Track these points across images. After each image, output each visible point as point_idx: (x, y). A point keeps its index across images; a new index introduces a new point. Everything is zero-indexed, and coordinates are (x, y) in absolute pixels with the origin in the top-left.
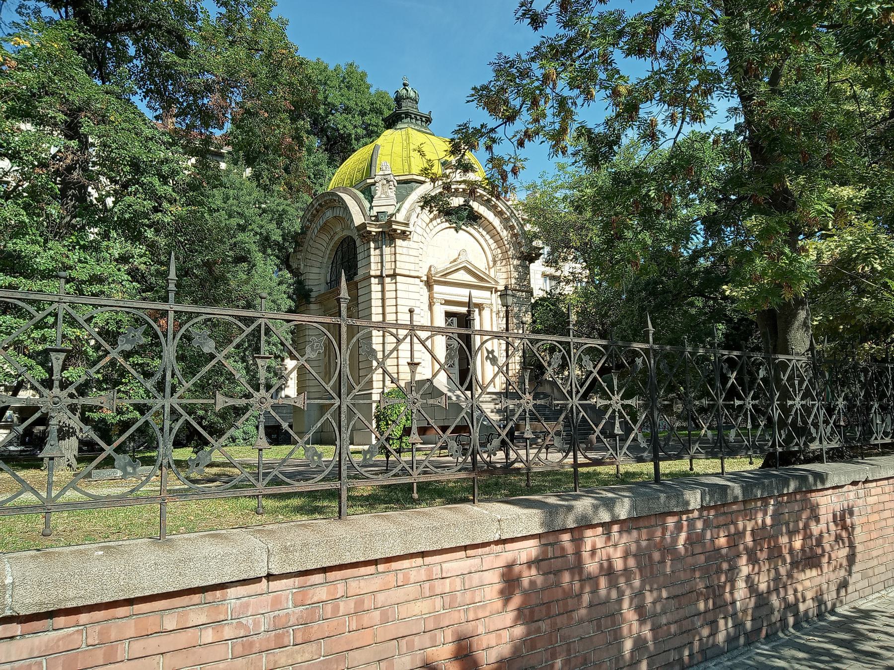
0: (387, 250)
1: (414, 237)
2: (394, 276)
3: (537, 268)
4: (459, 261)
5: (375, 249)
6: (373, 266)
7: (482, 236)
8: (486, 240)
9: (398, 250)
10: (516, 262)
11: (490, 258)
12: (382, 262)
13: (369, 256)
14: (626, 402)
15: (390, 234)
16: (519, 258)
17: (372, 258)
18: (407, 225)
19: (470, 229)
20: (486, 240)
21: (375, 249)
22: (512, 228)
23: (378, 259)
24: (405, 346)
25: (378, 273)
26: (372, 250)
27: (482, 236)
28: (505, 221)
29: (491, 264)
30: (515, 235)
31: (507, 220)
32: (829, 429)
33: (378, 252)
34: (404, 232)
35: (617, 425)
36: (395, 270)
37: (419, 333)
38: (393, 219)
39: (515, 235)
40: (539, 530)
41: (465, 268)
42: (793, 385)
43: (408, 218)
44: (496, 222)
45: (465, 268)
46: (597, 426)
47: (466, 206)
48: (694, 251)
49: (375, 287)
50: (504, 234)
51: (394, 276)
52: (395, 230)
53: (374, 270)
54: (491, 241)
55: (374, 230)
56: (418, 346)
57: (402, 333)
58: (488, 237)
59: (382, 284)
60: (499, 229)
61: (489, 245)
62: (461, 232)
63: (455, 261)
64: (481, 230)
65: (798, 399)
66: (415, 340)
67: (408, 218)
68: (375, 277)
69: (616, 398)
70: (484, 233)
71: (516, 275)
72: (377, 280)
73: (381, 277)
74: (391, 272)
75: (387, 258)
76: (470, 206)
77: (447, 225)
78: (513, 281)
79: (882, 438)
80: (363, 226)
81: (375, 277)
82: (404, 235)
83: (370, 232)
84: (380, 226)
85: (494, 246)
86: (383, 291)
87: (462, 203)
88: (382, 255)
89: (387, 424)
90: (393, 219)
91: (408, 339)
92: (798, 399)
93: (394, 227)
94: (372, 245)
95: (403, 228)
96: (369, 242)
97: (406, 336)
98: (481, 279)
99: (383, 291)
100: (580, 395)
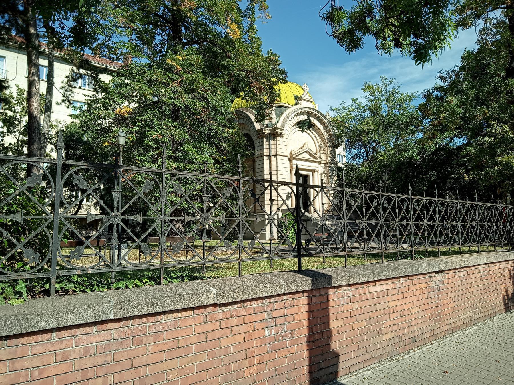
0: (272, 142)
1: (285, 136)
2: (276, 155)
3: (339, 150)
4: (304, 148)
5: (266, 141)
6: (265, 150)
7: (314, 135)
8: (316, 137)
9: (278, 142)
10: (330, 149)
11: (318, 147)
12: (270, 148)
13: (263, 145)
14: (369, 222)
15: (274, 134)
16: (332, 147)
17: (265, 146)
18: (283, 130)
19: (308, 131)
20: (316, 137)
21: (266, 141)
22: (329, 131)
23: (268, 147)
24: (267, 192)
25: (268, 154)
26: (264, 142)
27: (314, 135)
28: (326, 127)
29: (318, 150)
30: (330, 135)
31: (327, 127)
32: (463, 237)
33: (267, 143)
34: (281, 133)
35: (365, 233)
36: (276, 152)
37: (274, 184)
38: (275, 126)
39: (330, 135)
40: (331, 291)
41: (307, 152)
42: (423, 214)
43: (283, 126)
44: (321, 128)
45: (307, 152)
46: (373, 233)
47: (308, 120)
48: (440, 146)
49: (266, 161)
50: (325, 134)
51: (276, 155)
52: (277, 132)
53: (266, 152)
54: (318, 138)
55: (266, 132)
56: (274, 191)
57: (266, 184)
58: (317, 135)
59: (270, 160)
60: (323, 131)
61: (317, 140)
62: (304, 133)
63: (302, 147)
64: (313, 132)
65: (426, 221)
66: (273, 188)
67: (283, 126)
68: (266, 156)
69: (365, 219)
70: (315, 133)
71: (330, 155)
72: (267, 157)
73: (269, 156)
74: (275, 154)
75: (272, 146)
76: (310, 120)
77: (298, 129)
78: (329, 159)
79: (489, 242)
80: (261, 130)
81: (266, 156)
82: (281, 135)
83: (264, 133)
84: (270, 130)
85: (320, 140)
86: (270, 163)
87: (306, 118)
88: (269, 145)
89: (287, 230)
90: (275, 126)
91: (269, 188)
92: (426, 221)
93: (277, 131)
94: (265, 139)
95: (281, 132)
96: (262, 138)
97: (268, 187)
98: (314, 157)
99: (270, 163)
100: (348, 217)
